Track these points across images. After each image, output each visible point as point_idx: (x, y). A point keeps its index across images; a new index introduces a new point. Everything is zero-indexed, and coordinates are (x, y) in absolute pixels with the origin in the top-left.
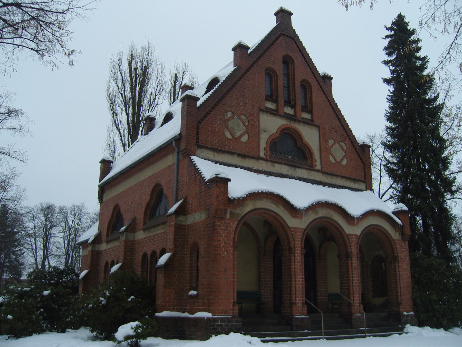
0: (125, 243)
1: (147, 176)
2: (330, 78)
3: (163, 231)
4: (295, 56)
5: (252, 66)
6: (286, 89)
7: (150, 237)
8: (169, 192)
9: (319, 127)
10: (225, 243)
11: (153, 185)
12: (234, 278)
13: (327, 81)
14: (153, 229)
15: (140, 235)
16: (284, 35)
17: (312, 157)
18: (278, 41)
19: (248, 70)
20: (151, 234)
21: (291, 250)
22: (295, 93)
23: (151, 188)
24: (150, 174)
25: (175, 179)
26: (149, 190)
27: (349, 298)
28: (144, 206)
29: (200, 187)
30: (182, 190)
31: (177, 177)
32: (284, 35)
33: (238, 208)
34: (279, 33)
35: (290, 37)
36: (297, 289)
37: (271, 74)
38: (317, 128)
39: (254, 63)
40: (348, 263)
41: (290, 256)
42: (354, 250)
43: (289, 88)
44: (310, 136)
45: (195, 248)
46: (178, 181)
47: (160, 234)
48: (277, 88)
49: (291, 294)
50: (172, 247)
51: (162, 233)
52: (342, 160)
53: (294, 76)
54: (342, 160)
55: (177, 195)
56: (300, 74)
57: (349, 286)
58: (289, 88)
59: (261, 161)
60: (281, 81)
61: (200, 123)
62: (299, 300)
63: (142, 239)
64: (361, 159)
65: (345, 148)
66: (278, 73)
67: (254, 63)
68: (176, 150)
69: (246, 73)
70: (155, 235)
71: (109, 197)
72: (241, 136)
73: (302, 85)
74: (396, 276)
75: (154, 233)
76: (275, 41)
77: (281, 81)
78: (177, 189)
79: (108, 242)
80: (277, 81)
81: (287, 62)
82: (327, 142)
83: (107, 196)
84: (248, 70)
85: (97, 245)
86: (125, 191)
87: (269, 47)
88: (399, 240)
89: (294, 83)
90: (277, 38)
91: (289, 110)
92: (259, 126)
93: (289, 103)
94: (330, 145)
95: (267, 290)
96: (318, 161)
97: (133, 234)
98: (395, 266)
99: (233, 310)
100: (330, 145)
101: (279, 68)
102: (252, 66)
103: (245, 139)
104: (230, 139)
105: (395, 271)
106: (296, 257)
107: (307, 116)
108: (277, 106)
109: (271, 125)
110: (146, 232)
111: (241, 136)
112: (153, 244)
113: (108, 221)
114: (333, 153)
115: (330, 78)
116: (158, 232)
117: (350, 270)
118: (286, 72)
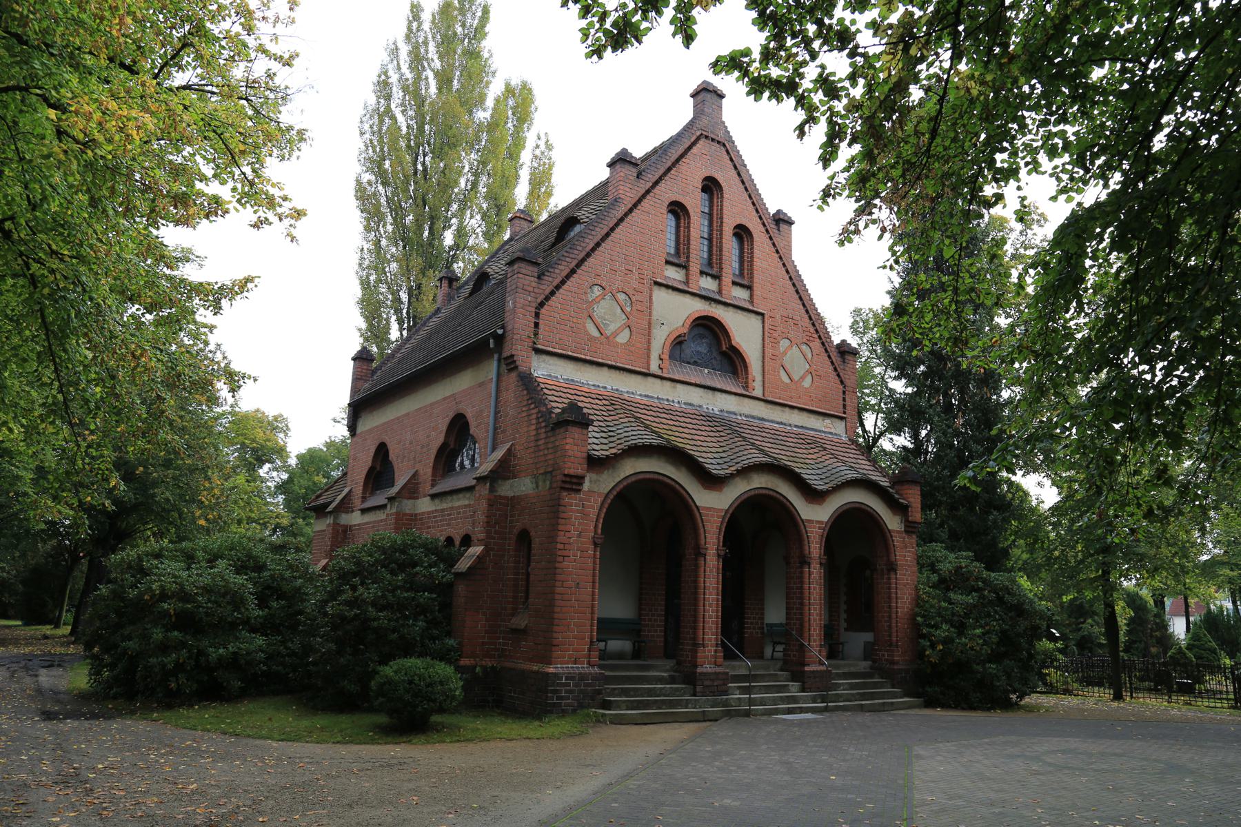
0: (396, 519)
1: (440, 398)
2: (790, 223)
3: (467, 502)
4: (726, 177)
5: (644, 196)
6: (706, 242)
7: (442, 510)
8: (480, 428)
9: (763, 315)
10: (579, 536)
11: (451, 415)
12: (593, 600)
13: (783, 226)
14: (449, 498)
15: (424, 505)
16: (707, 137)
17: (747, 373)
18: (695, 150)
19: (635, 206)
20: (444, 506)
21: (699, 553)
22: (721, 250)
23: (448, 420)
24: (447, 394)
25: (492, 410)
26: (443, 425)
27: (801, 635)
28: (434, 452)
29: (537, 429)
30: (504, 432)
31: (496, 407)
32: (707, 137)
33: (555, 635)
34: (698, 133)
35: (719, 142)
36: (707, 619)
37: (678, 210)
38: (760, 318)
39: (648, 192)
40: (802, 572)
41: (696, 559)
42: (815, 548)
43: (713, 241)
44: (744, 333)
45: (524, 538)
46: (496, 413)
47: (458, 507)
48: (689, 240)
49: (695, 628)
50: (482, 536)
51: (466, 506)
52: (803, 378)
53: (722, 218)
54: (803, 378)
55: (494, 439)
56: (735, 211)
57: (801, 614)
58: (713, 241)
59: (651, 380)
60: (698, 226)
61: (542, 305)
62: (710, 640)
63: (429, 513)
64: (838, 375)
65: (809, 356)
66: (691, 211)
67: (648, 192)
68: (496, 356)
69: (631, 210)
70: (452, 508)
71: (367, 427)
72: (615, 334)
73: (735, 234)
74: (890, 597)
75: (450, 505)
76: (690, 148)
77: (698, 226)
78: (495, 429)
79: (364, 511)
80: (689, 227)
81: (711, 186)
82: (775, 343)
83: (365, 425)
84: (635, 206)
85: (344, 516)
86: (398, 418)
87: (677, 161)
88: (898, 532)
89: (721, 231)
90: (694, 144)
91: (708, 284)
92: (650, 314)
93: (713, 269)
94: (782, 350)
95: (653, 615)
96: (759, 378)
97: (411, 501)
98: (889, 579)
99: (589, 656)
100: (782, 350)
101: (695, 202)
102: (644, 196)
103: (623, 338)
104: (595, 338)
105: (889, 588)
106: (708, 562)
107: (740, 294)
108: (687, 275)
109: (674, 312)
110: (437, 501)
111: (615, 334)
112: (449, 525)
113: (365, 472)
114: (788, 366)
115: (790, 223)
116: (457, 504)
117: (806, 586)
118: (706, 210)
